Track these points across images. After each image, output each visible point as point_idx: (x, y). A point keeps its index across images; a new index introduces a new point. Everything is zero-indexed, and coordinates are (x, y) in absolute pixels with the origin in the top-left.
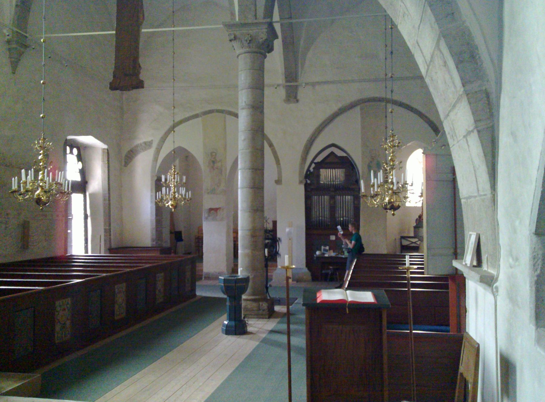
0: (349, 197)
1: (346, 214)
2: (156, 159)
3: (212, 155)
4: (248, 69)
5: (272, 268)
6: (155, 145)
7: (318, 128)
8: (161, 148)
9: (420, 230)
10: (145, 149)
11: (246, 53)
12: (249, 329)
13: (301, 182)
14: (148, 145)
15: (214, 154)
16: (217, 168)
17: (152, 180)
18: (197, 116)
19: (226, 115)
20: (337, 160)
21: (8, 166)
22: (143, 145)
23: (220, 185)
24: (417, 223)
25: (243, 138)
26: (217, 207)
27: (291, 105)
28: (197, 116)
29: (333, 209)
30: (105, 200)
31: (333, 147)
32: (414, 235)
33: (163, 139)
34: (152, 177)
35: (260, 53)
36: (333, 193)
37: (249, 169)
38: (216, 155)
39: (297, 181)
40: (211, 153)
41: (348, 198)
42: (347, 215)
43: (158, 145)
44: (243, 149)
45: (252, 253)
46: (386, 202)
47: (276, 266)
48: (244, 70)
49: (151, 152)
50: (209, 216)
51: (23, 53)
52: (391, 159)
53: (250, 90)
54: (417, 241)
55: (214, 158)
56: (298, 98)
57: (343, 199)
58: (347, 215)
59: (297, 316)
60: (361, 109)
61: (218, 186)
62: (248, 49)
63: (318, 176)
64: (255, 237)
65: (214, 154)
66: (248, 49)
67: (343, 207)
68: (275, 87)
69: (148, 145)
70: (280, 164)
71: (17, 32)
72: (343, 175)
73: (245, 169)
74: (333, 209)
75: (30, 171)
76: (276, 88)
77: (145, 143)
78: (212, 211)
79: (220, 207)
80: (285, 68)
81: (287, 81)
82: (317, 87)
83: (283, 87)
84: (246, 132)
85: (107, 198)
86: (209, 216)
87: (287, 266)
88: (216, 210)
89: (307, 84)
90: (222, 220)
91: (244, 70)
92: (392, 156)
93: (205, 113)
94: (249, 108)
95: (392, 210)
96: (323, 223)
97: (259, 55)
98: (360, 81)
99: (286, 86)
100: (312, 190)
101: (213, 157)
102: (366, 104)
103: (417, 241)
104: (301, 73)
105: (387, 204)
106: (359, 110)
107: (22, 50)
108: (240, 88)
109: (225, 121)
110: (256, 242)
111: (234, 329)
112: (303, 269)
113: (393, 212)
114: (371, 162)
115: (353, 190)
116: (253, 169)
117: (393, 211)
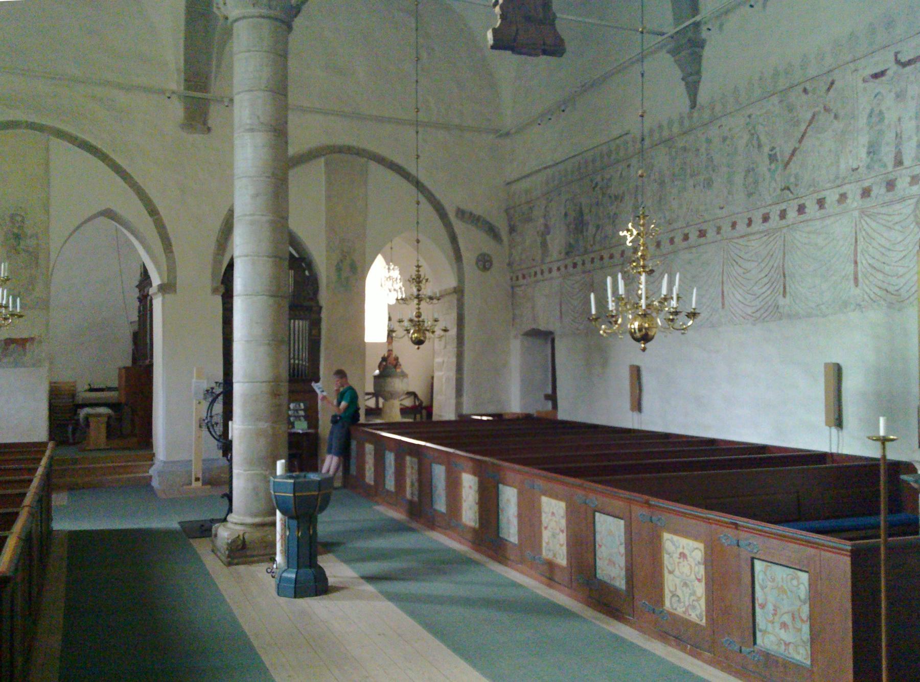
0: (301, 322)
1: (299, 355)
4: (265, 51)
5: (137, 463)
9: (387, 381)
11: (263, 17)
12: (331, 581)
13: (215, 291)
15: (19, 219)
16: (26, 251)
19: (51, 137)
24: (382, 369)
26: (25, 335)
27: (196, 136)
31: (290, 226)
32: (375, 390)
38: (23, 222)
39: (209, 289)
40: (12, 217)
41: (299, 324)
42: (296, 357)
44: (251, 215)
45: (273, 428)
46: (634, 329)
47: (152, 457)
48: (257, 51)
52: (641, 256)
53: (267, 93)
55: (19, 227)
56: (210, 123)
57: (294, 326)
58: (296, 357)
59: (350, 546)
60: (327, 164)
62: (264, 11)
64: (279, 395)
66: (264, 11)
67: (294, 343)
68: (168, 95)
70: (172, 252)
73: (258, 256)
76: (169, 98)
78: (13, 346)
79: (33, 336)
80: (186, 61)
81: (188, 88)
83: (179, 97)
84: (262, 179)
87: (883, 437)
90: (37, 364)
91: (257, 51)
92: (643, 250)
94: (266, 131)
95: (642, 342)
96: (296, 369)
99: (186, 97)
101: (17, 225)
102: (336, 156)
104: (216, 77)
105: (637, 331)
106: (323, 164)
111: (293, 585)
112: (217, 460)
113: (643, 346)
114: (342, 261)
115: (309, 309)
116: (276, 257)
117: (644, 344)
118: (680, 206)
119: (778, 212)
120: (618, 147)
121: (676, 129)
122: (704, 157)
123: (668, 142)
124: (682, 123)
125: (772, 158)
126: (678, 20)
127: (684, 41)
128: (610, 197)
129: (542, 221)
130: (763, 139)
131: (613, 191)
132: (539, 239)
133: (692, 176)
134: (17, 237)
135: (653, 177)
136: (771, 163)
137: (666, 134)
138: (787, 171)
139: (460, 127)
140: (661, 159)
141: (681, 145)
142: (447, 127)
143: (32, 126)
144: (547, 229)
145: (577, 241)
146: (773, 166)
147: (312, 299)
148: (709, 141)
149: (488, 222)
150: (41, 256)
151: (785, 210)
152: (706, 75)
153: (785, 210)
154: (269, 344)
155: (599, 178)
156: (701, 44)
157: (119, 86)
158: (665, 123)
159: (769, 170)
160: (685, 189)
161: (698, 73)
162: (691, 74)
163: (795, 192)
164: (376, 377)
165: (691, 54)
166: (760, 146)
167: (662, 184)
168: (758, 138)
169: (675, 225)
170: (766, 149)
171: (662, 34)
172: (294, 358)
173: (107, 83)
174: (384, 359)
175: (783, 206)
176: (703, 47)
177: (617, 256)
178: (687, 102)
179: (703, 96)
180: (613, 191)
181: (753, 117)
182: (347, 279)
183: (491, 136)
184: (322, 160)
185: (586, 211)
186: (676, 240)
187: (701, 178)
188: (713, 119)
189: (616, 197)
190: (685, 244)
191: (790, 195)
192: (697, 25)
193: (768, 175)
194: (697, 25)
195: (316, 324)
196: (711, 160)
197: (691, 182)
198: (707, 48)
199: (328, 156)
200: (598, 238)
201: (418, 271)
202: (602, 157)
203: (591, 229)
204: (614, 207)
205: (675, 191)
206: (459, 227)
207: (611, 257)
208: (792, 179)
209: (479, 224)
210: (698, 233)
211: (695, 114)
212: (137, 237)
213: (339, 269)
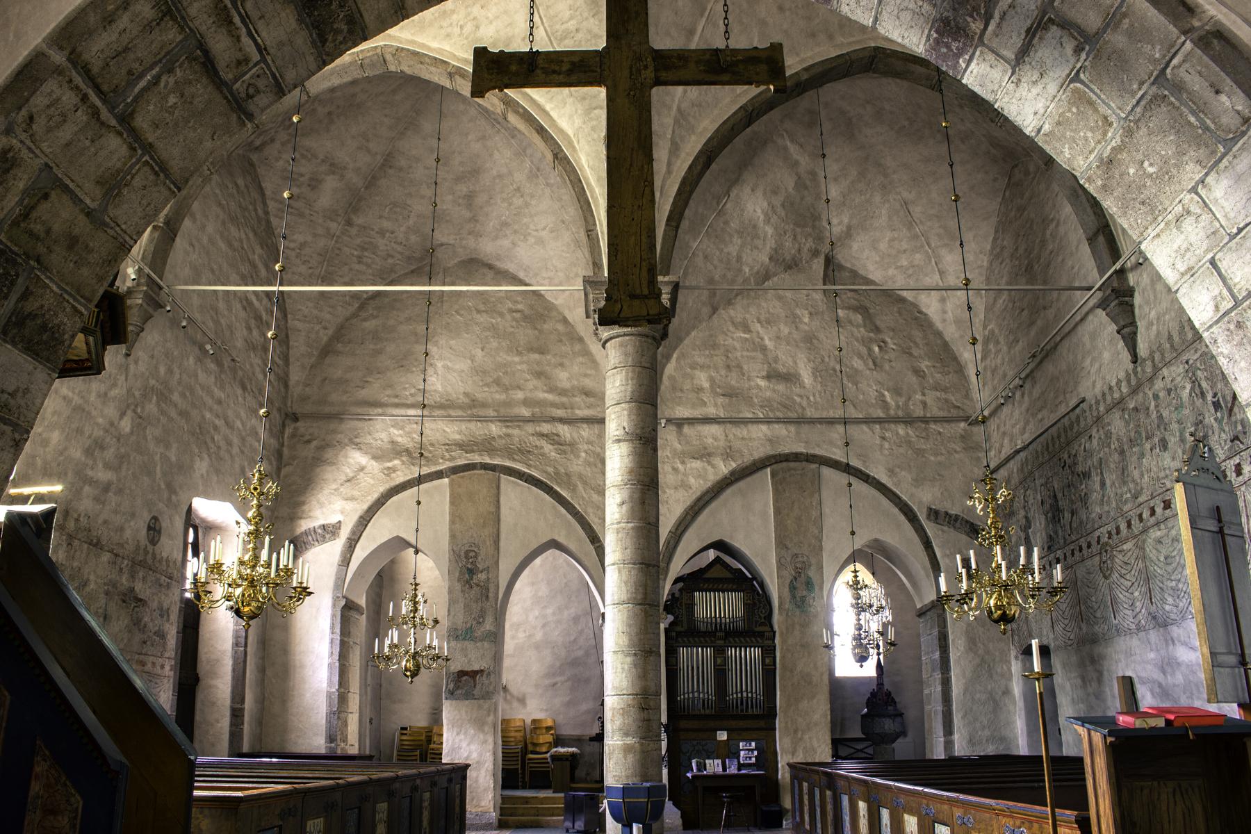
2: (346, 561)
3: (467, 557)
6: (345, 533)
7: (691, 507)
8: (359, 538)
10: (322, 540)
14: (330, 531)
17: (334, 606)
18: (439, 475)
20: (728, 575)
21: (94, 546)
22: (320, 531)
23: (483, 621)
25: (618, 499)
26: (476, 667)
28: (439, 475)
29: (721, 673)
30: (236, 644)
33: (364, 521)
34: (335, 600)
35: (654, 338)
36: (721, 642)
37: (634, 564)
38: (476, 557)
40: (467, 552)
43: (353, 532)
44: (619, 523)
45: (642, 745)
49: (333, 549)
50: (457, 687)
51: (151, 317)
54: (1223, 654)
61: (479, 623)
63: (691, 606)
65: (472, 554)
69: (330, 531)
71: (148, 276)
72: (740, 605)
74: (721, 673)
75: (213, 542)
77: (324, 527)
82: (686, 429)
85: (243, 640)
86: (457, 687)
88: (473, 674)
89: (669, 421)
93: (455, 470)
97: (650, 341)
98: (768, 421)
100: (679, 634)
103: (1223, 654)
107: (151, 310)
108: (608, 402)
109: (498, 487)
110: (649, 720)
115: (761, 634)
118: (1142, 475)
119: (1233, 468)
120: (1078, 417)
121: (1125, 390)
122: (1154, 416)
123: (1119, 404)
124: (1129, 381)
125: (1217, 406)
126: (1102, 272)
127: (1109, 291)
128: (1079, 475)
129: (1022, 513)
130: (1204, 385)
131: (1080, 468)
132: (1023, 535)
133: (1147, 439)
134: (471, 572)
135: (1113, 447)
136: (1216, 411)
137: (1116, 395)
138: (1233, 419)
139: (925, 420)
140: (1117, 425)
141: (1131, 406)
142: (908, 421)
143: (485, 467)
144: (1028, 523)
145: (1056, 533)
146: (1219, 414)
147: (762, 624)
148: (1156, 397)
149: (967, 522)
150: (492, 590)
151: (1239, 465)
152: (1141, 325)
153: (1239, 465)
154: (635, 654)
155: (1066, 456)
156: (1130, 292)
157: (562, 420)
158: (1113, 384)
159: (1216, 419)
160: (1142, 455)
161: (1133, 323)
162: (1124, 327)
163: (1244, 441)
164: (863, 716)
165: (1121, 304)
166: (1203, 394)
167: (1122, 452)
168: (1200, 385)
169: (1140, 500)
170: (1209, 397)
171: (1089, 289)
172: (737, 693)
173: (553, 420)
174: (873, 694)
175: (1237, 460)
176: (1132, 296)
177: (1094, 543)
178: (1126, 356)
179: (1143, 349)
180: (1080, 468)
181: (1191, 362)
182: (803, 599)
183: (962, 425)
184: (769, 470)
185: (1060, 495)
186: (1144, 516)
187: (1156, 440)
188: (1156, 370)
189: (1084, 474)
190: (1153, 520)
191: (1241, 446)
192: (1121, 272)
193: (1215, 425)
194: (1121, 272)
195: (769, 651)
196: (1160, 417)
197: (1148, 446)
198: (1136, 294)
199: (775, 466)
200: (1074, 525)
201: (856, 577)
202: (1065, 431)
203: (1067, 515)
204: (1083, 486)
205: (1134, 458)
206: (930, 529)
207: (1089, 546)
208: (1240, 428)
209: (958, 525)
210: (1162, 505)
211: (1139, 369)
212: (580, 564)
213: (793, 588)
